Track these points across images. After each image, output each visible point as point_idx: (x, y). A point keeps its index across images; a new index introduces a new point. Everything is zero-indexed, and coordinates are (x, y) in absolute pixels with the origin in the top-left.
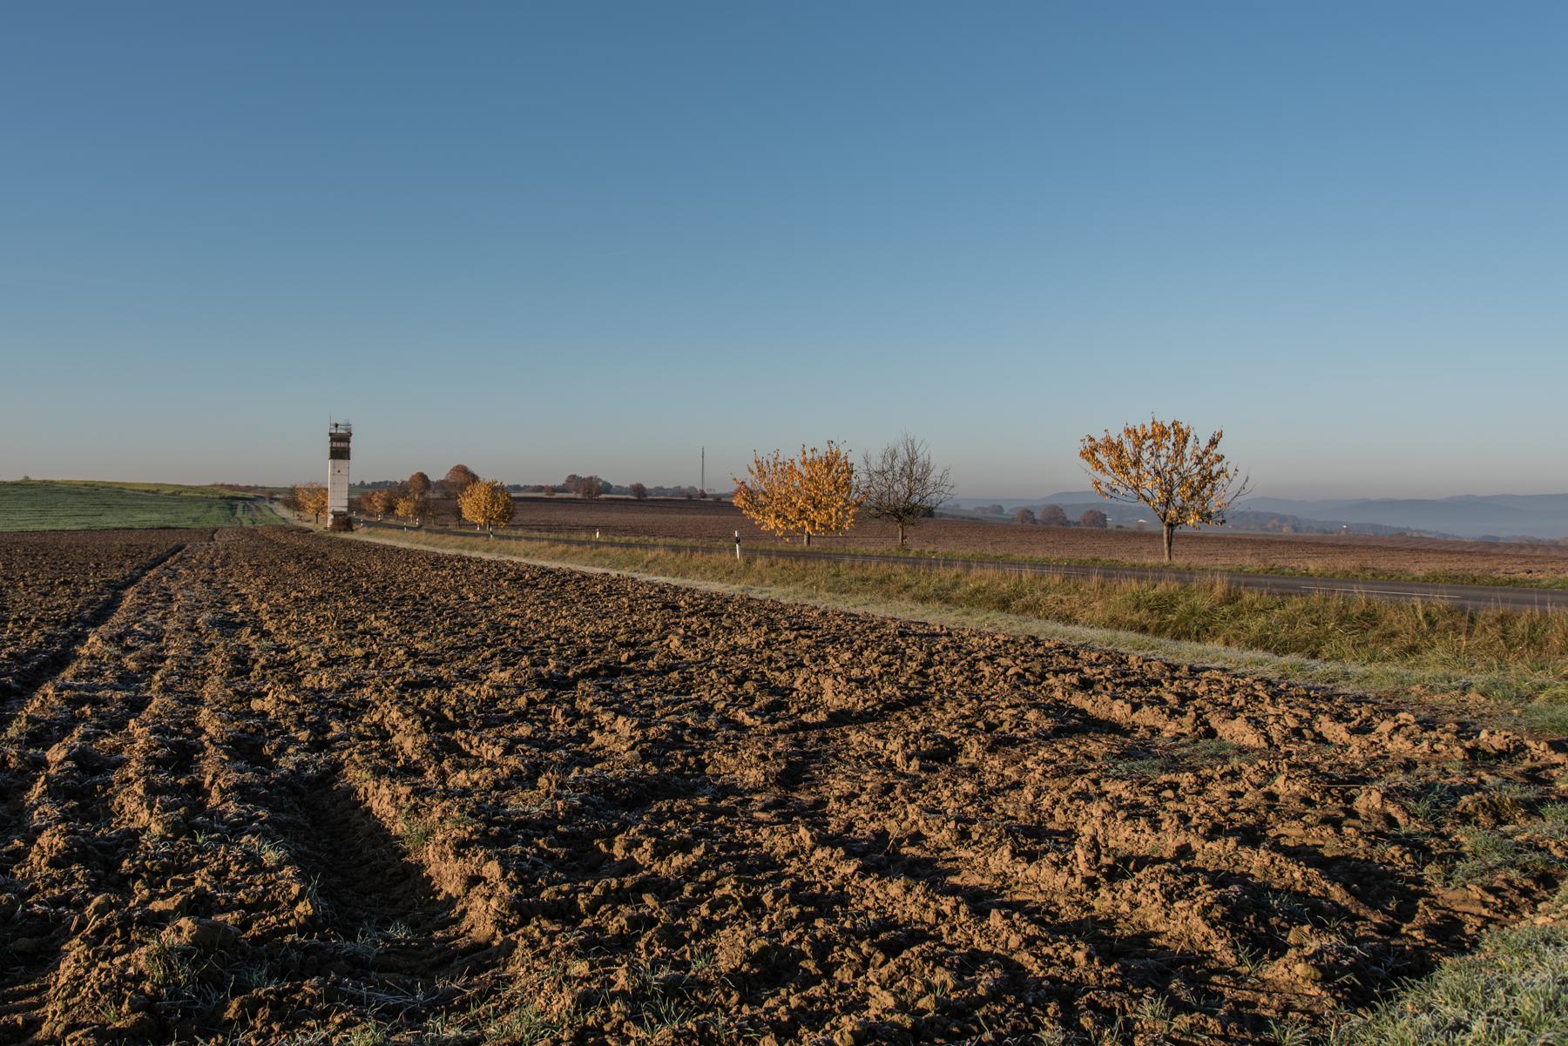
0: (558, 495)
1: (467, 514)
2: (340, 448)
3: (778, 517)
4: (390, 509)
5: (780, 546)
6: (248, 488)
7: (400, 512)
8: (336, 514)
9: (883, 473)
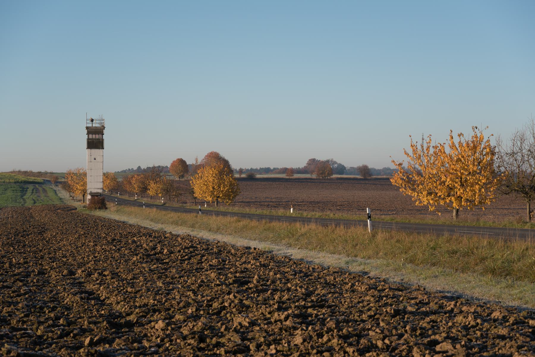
0: (296, 176)
1: (198, 194)
2: (95, 141)
3: (430, 194)
4: (144, 189)
5: (429, 219)
6: (40, 174)
7: (151, 193)
8: (93, 195)
9: (513, 154)
